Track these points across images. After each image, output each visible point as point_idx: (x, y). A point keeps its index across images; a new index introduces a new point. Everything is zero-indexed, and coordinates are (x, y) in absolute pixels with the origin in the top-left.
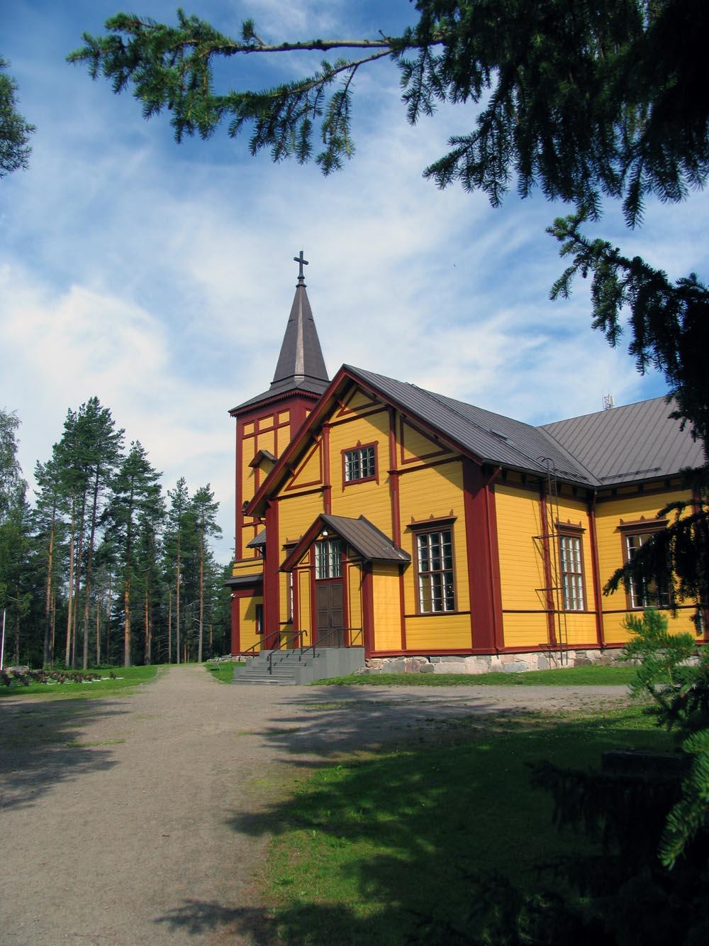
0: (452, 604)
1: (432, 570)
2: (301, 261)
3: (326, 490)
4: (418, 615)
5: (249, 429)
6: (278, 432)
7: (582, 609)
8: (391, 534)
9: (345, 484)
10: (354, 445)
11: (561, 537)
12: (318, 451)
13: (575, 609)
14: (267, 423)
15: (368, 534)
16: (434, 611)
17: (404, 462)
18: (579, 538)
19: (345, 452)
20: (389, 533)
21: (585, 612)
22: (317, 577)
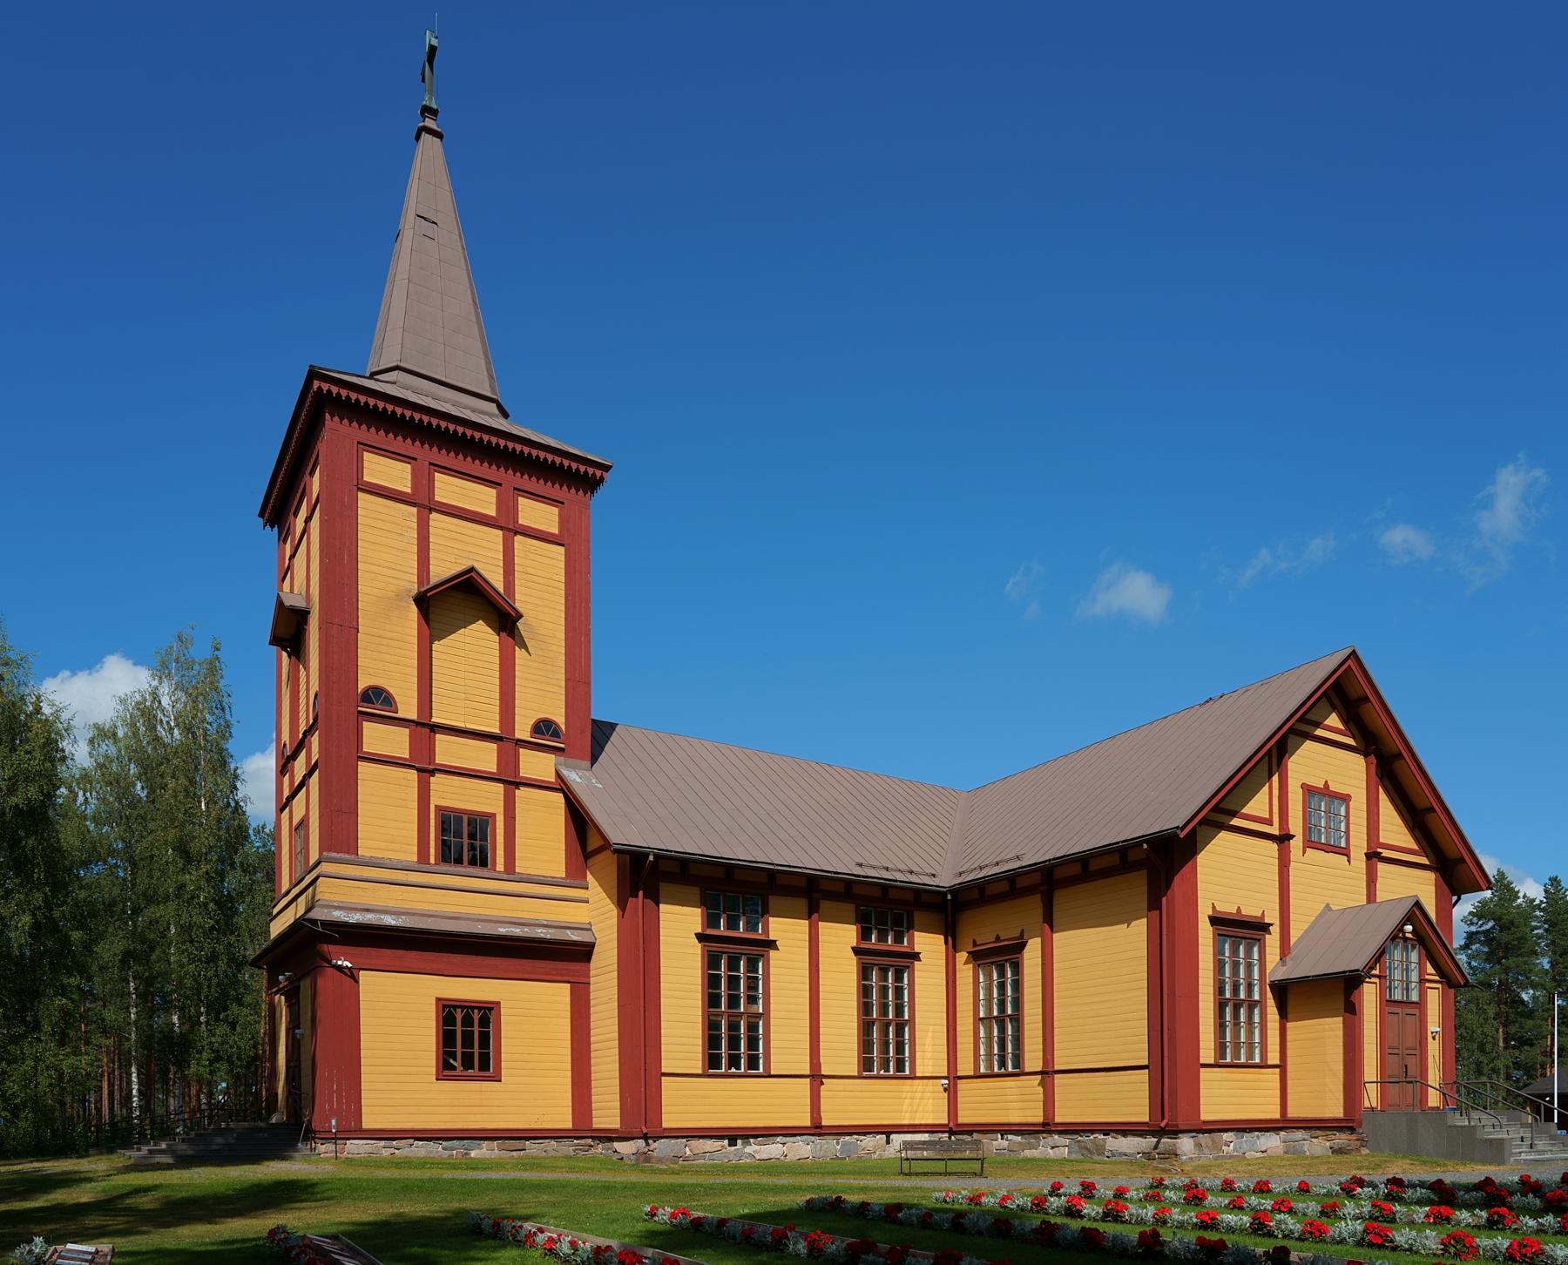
0: (1018, 1060)
1: (1009, 1012)
4: (978, 1076)
7: (1257, 1060)
11: (1219, 937)
13: (1243, 1060)
16: (1010, 1069)
18: (1259, 940)
21: (1263, 1065)
22: (982, 1015)
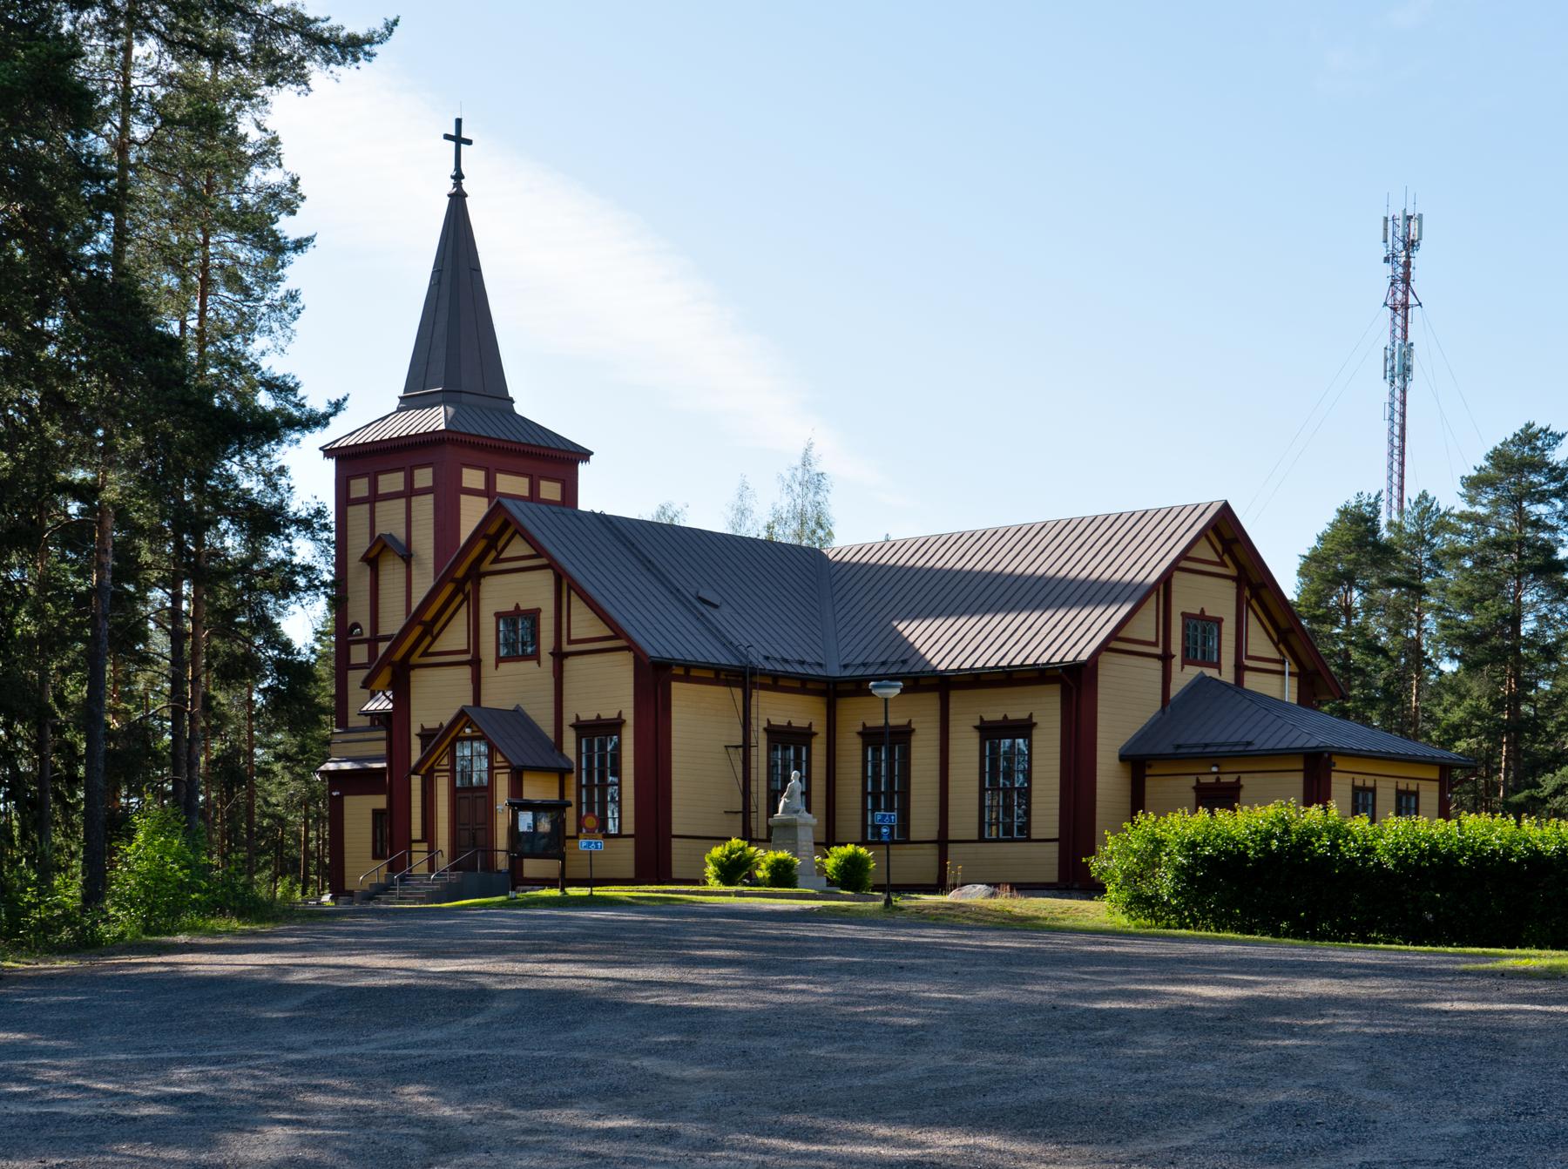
2: (458, 140)
3: (475, 663)
5: (360, 488)
6: (413, 504)
8: (552, 729)
9: (499, 660)
10: (511, 608)
12: (464, 609)
14: (392, 482)
15: (673, 571)
17: (570, 642)
19: (498, 616)
20: (548, 729)
21: (619, 835)
